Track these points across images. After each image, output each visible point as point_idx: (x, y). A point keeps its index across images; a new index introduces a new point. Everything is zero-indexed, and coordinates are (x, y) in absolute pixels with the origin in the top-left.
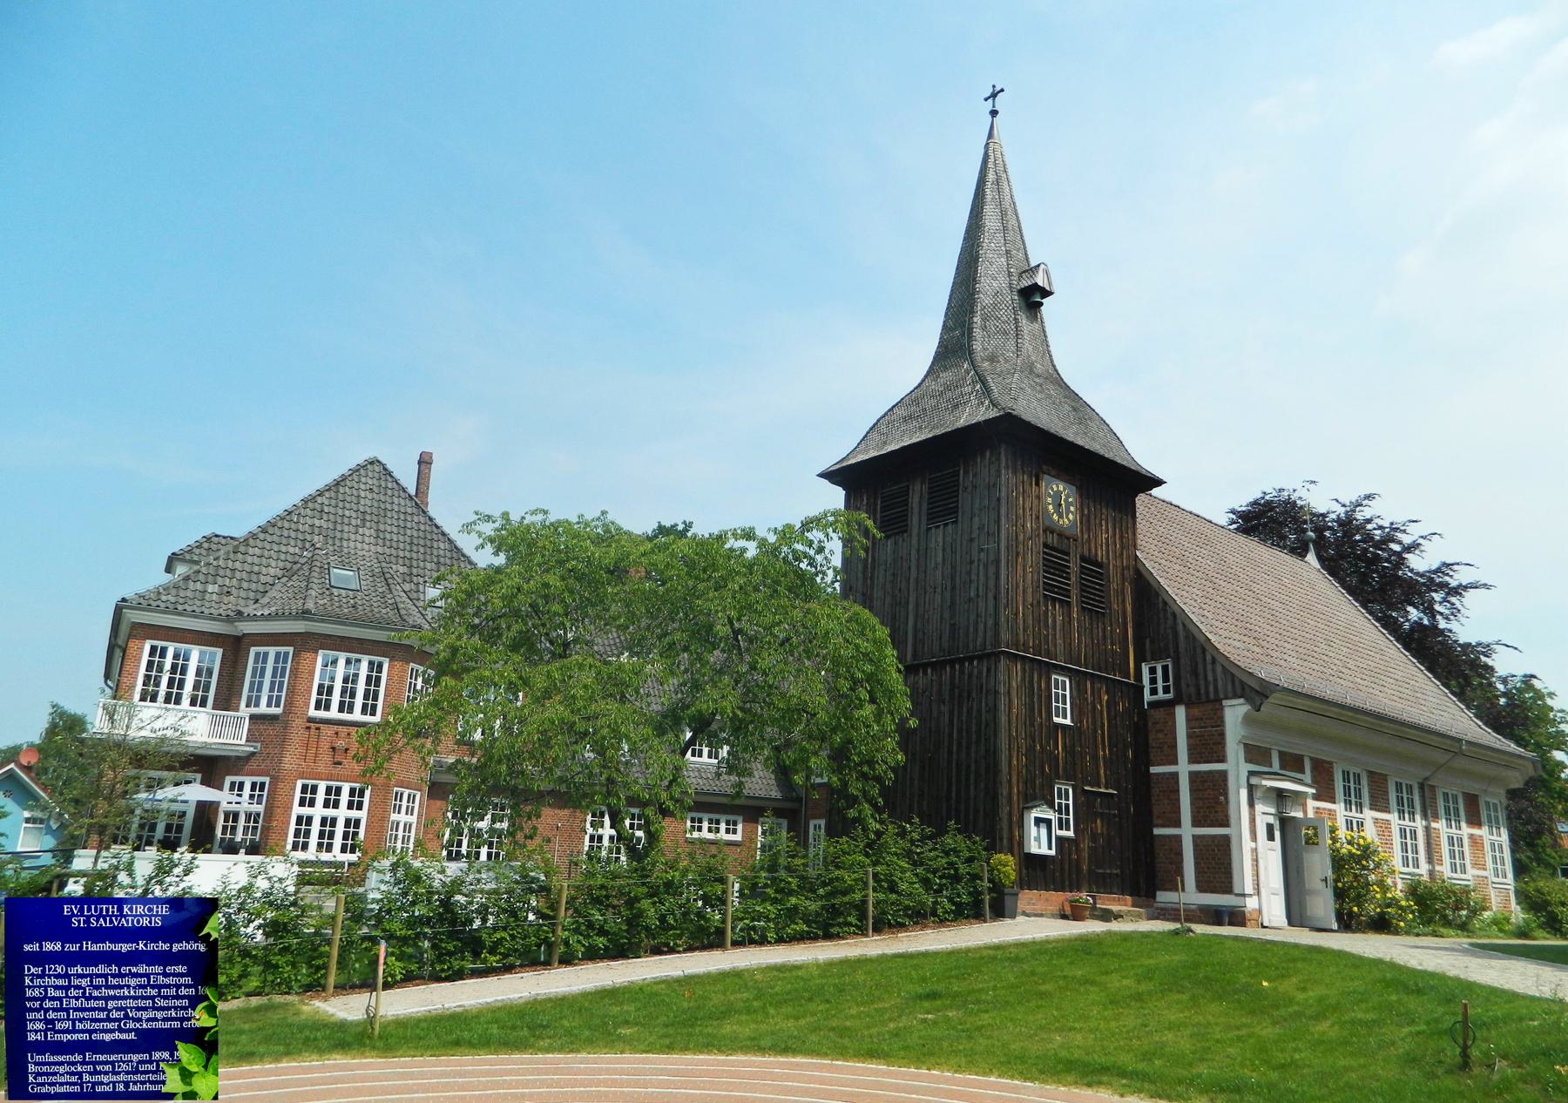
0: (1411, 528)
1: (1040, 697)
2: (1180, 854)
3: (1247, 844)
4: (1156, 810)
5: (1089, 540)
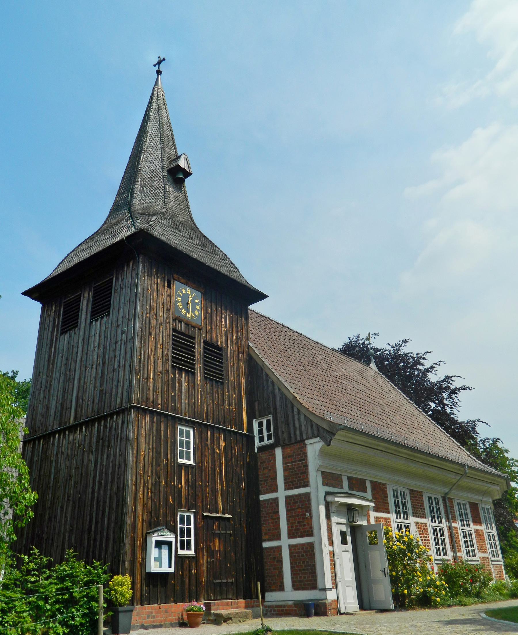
0: (427, 356)
1: (166, 443)
2: (280, 561)
3: (326, 549)
4: (264, 528)
5: (211, 330)
